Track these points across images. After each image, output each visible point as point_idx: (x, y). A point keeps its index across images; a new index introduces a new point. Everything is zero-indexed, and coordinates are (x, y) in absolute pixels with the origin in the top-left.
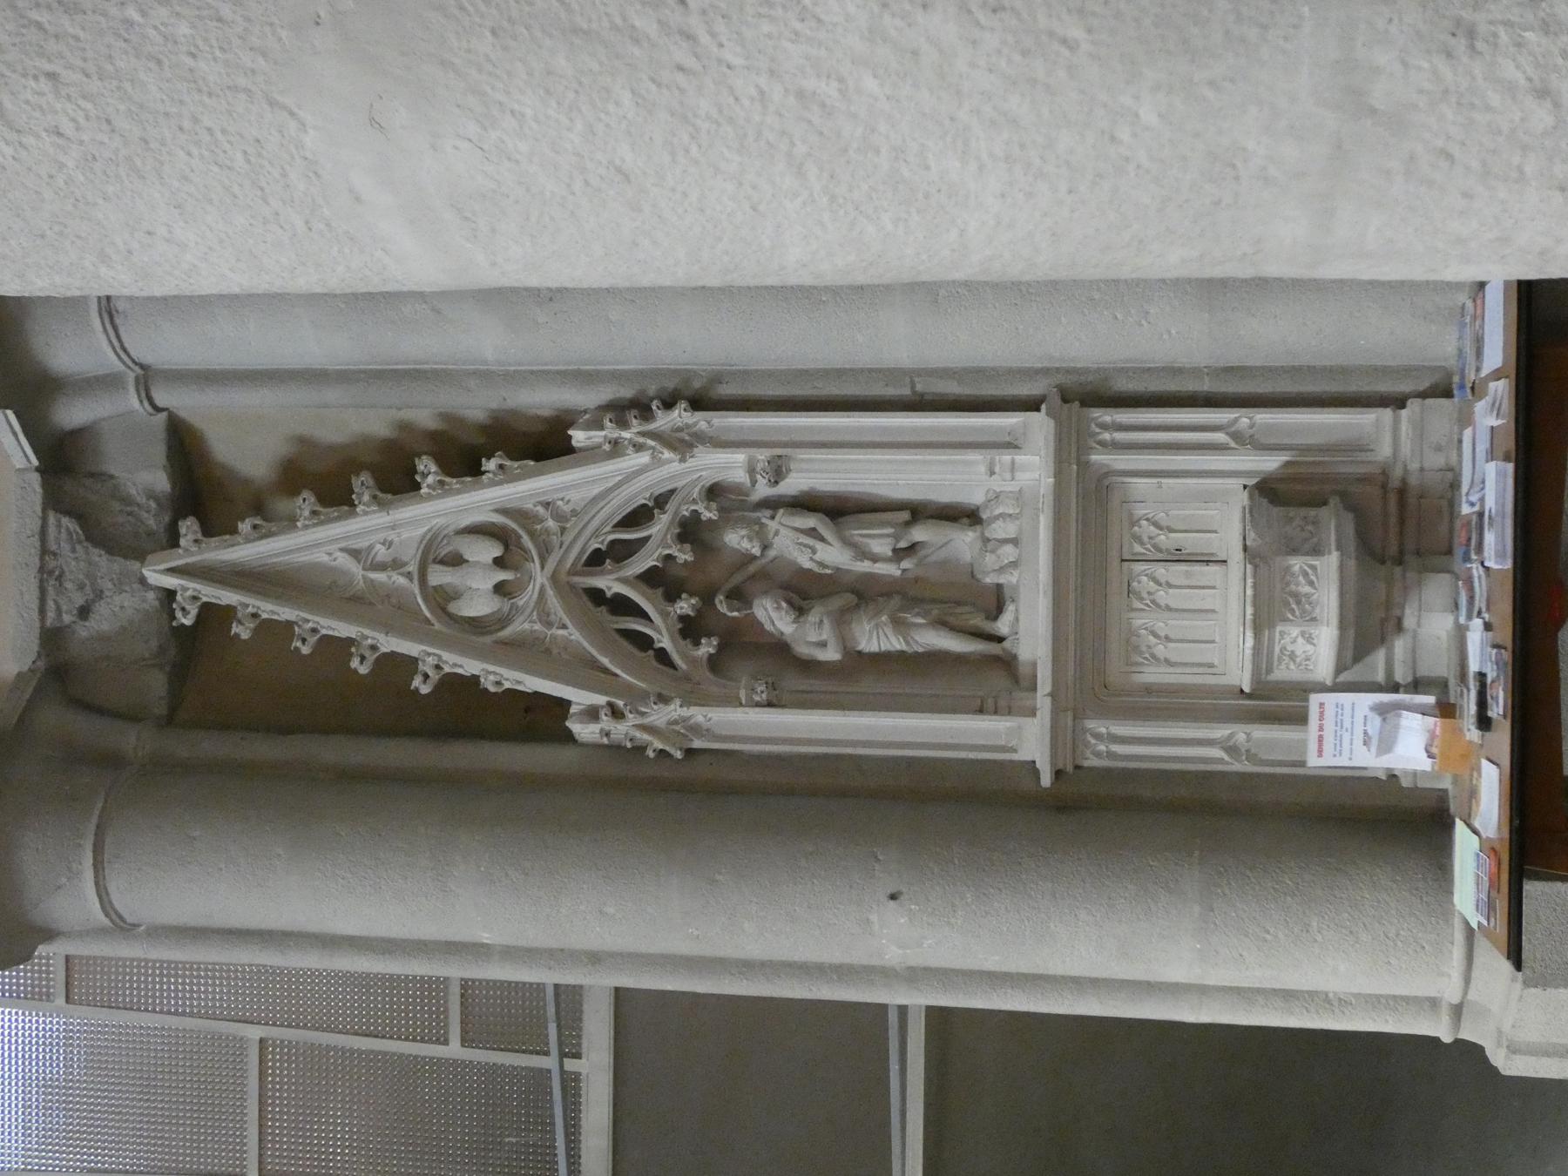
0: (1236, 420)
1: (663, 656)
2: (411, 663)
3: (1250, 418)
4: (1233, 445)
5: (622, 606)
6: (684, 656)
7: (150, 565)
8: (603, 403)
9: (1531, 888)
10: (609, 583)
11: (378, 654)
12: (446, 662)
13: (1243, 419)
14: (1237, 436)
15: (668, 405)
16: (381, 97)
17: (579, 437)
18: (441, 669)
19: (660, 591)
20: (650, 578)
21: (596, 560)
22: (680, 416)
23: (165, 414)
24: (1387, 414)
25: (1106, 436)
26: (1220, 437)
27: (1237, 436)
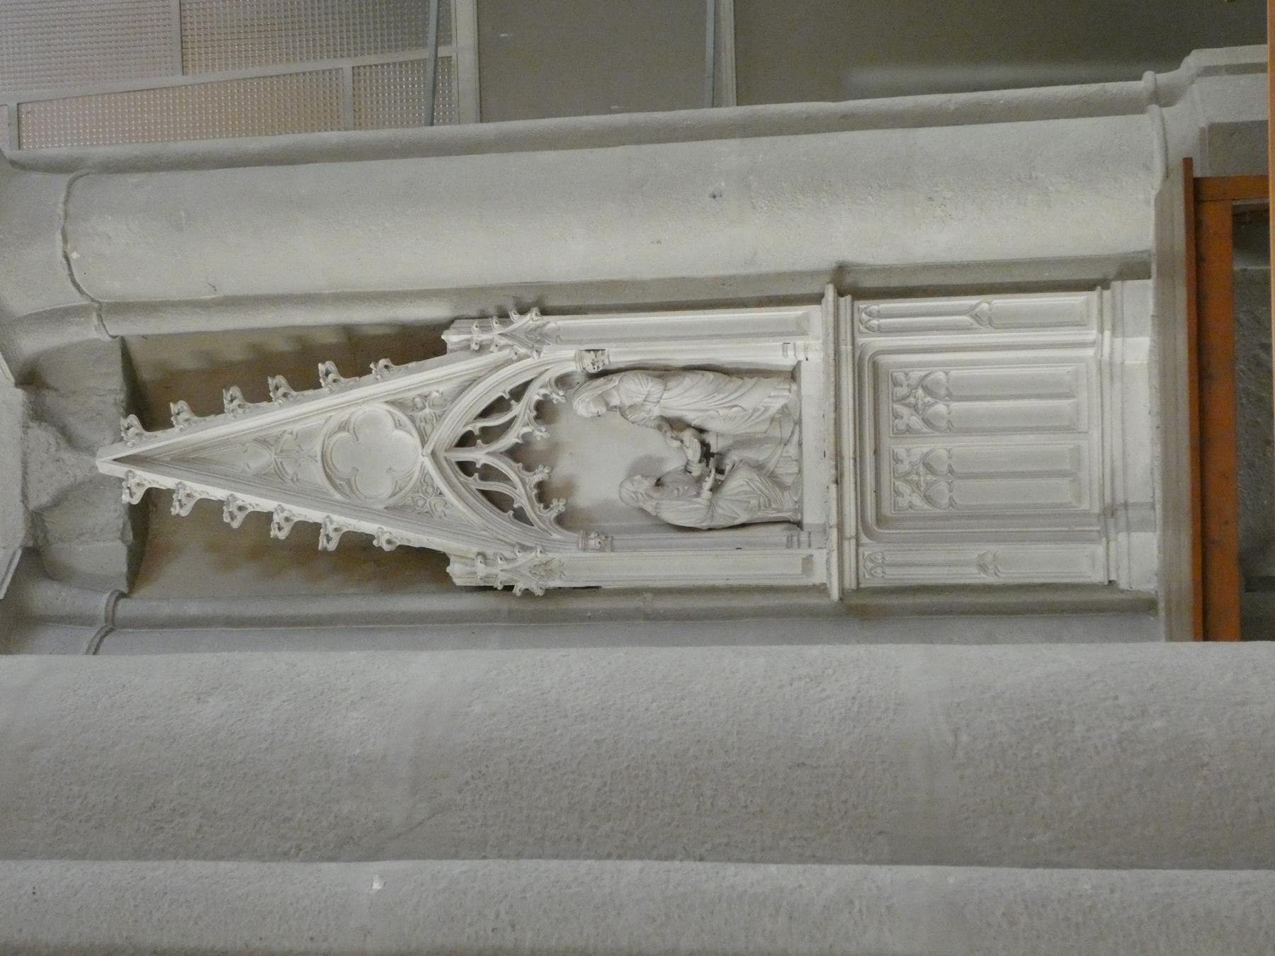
0: (979, 303)
1: (520, 516)
2: (316, 527)
3: (989, 303)
4: (976, 325)
5: (488, 473)
6: (540, 518)
7: (100, 457)
8: (667, 417)
9: (855, 302)
10: (478, 455)
11: (196, 501)
12: (196, 491)
13: (984, 303)
14: (977, 317)
15: (523, 311)
16: (824, 441)
17: (450, 338)
18: (143, 485)
19: (520, 465)
20: (514, 453)
21: (466, 440)
22: (532, 319)
23: (118, 338)
24: (1093, 296)
25: (875, 322)
26: (965, 319)
27: (977, 317)
